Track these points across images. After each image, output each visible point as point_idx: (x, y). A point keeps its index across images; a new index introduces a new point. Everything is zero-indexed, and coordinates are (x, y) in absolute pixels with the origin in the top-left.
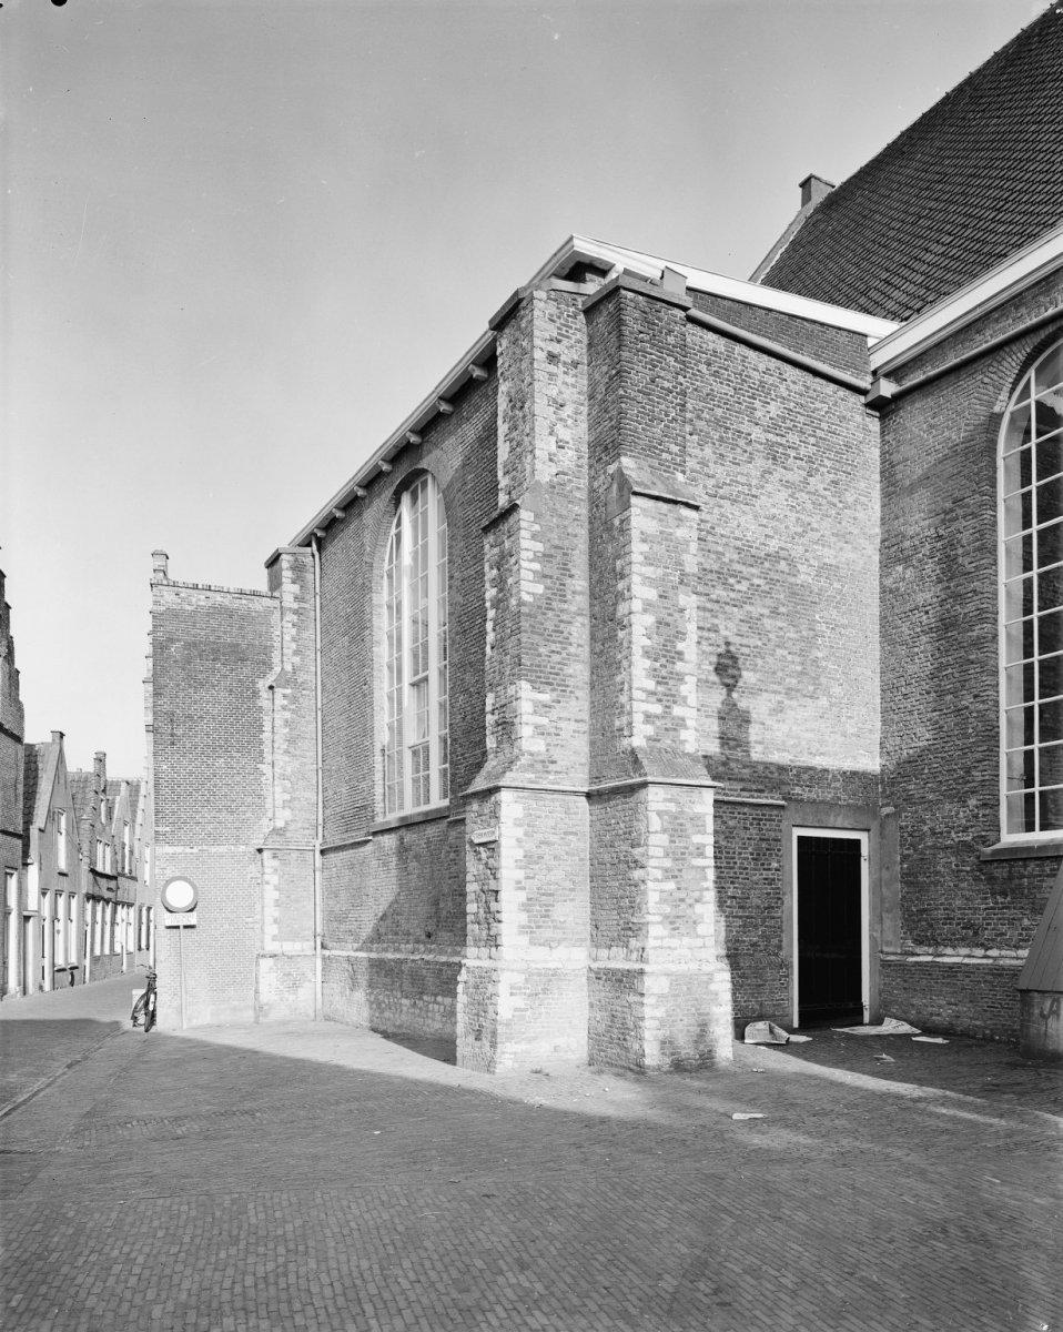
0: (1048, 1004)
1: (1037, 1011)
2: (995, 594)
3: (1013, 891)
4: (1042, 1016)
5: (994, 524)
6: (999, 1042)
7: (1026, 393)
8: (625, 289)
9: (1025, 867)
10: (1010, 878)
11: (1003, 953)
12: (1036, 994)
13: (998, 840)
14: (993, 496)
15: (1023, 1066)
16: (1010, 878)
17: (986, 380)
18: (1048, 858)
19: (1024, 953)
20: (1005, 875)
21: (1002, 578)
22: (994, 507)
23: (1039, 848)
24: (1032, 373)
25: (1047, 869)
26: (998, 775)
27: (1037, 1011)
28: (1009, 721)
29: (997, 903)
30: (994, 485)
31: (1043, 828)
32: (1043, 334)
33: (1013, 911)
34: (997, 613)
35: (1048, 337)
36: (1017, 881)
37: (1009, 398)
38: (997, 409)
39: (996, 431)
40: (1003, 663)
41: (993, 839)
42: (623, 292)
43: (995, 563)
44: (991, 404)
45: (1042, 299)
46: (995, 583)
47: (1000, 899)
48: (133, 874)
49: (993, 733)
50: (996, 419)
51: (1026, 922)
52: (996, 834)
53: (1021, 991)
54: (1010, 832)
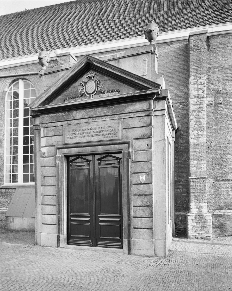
0: (12, 219)
1: (9, 221)
2: (4, 130)
3: (6, 195)
4: (10, 222)
5: (4, 115)
6: (3, 228)
7: (11, 89)
8: (161, 87)
9: (9, 190)
10: (6, 192)
11: (4, 209)
12: (9, 217)
13: (4, 184)
14: (4, 109)
15: (5, 233)
16: (6, 192)
17: (3, 83)
18: (13, 188)
19: (7, 208)
20: (5, 192)
21: (6, 127)
22: (4, 111)
23: (12, 186)
24: (12, 85)
25: (13, 191)
26: (4, 170)
27: (9, 221)
28: (6, 158)
29: (3, 198)
30: (4, 107)
31: (13, 182)
32: (16, 78)
33: (6, 199)
34: (4, 135)
35: (16, 79)
36: (7, 193)
37: (8, 88)
38: (5, 90)
39: (5, 95)
40: (5, 145)
41: (2, 184)
42: (160, 87)
43: (4, 124)
44: (4, 89)
45: (15, 70)
46: (4, 128)
47: (3, 197)
48: (43, 177)
49: (3, 161)
50: (5, 92)
51: (9, 202)
52: (3, 182)
53: (6, 217)
54: (6, 182)
